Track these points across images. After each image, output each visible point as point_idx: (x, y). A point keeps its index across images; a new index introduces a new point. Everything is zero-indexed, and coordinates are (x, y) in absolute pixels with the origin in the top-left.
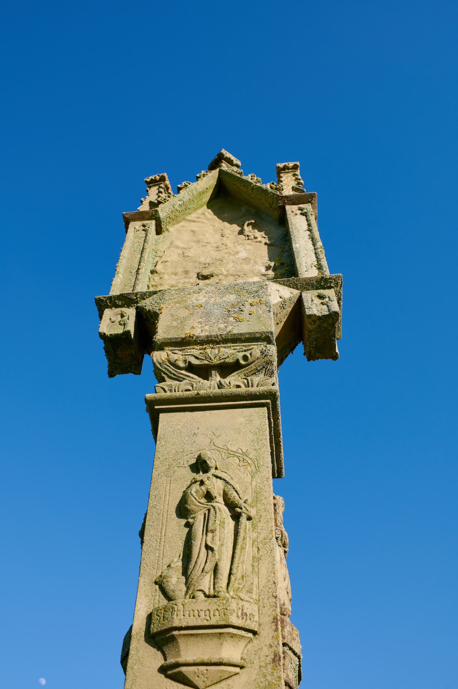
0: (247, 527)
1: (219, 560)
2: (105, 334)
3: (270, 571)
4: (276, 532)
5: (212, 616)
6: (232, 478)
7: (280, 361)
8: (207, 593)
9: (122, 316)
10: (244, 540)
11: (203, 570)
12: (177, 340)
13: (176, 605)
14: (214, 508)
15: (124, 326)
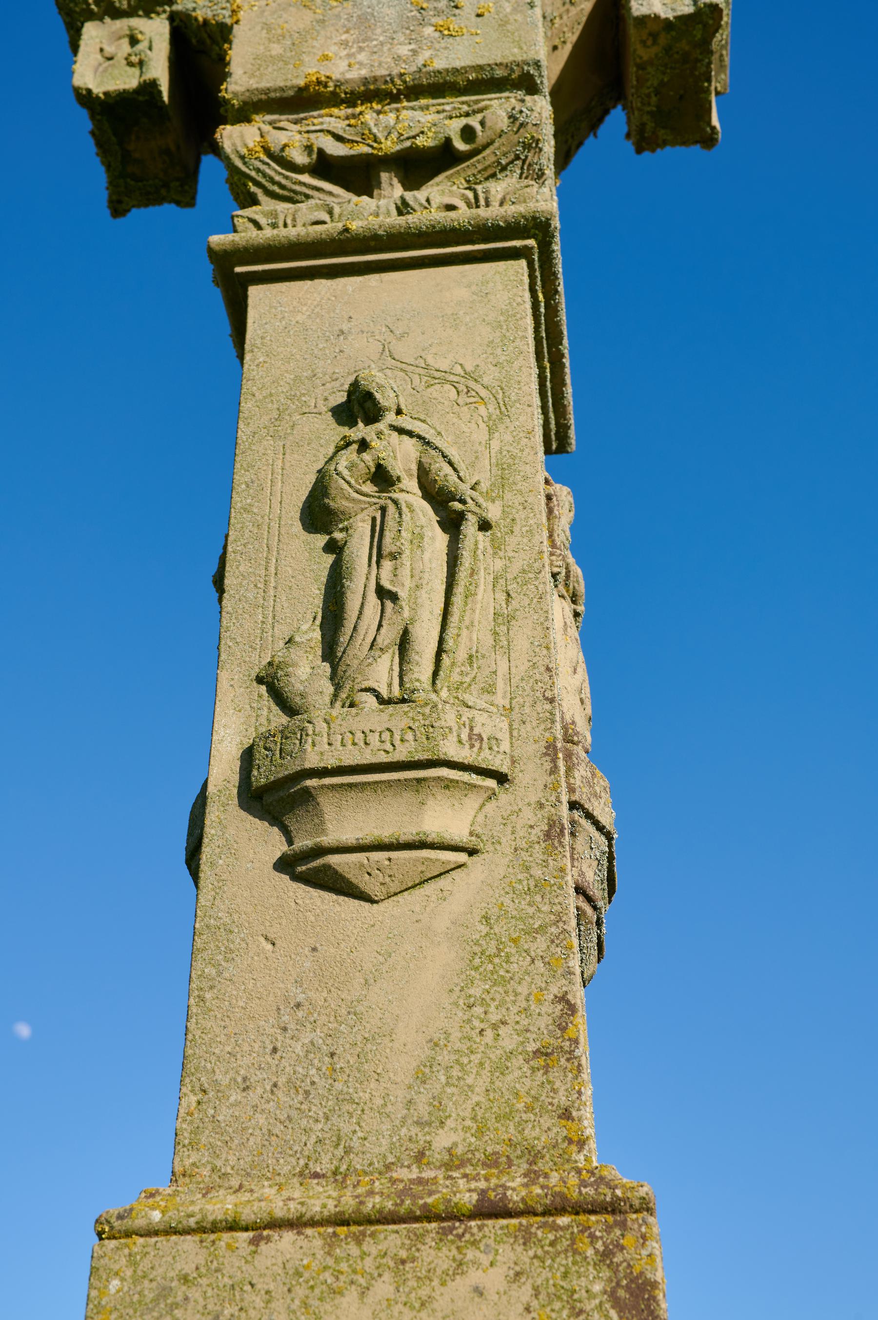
0: (481, 546)
1: (412, 620)
2: (89, 91)
3: (536, 644)
4: (552, 561)
5: (397, 743)
6: (439, 433)
7: (563, 159)
8: (385, 694)
9: (134, 41)
10: (472, 575)
11: (372, 645)
12: (285, 95)
13: (309, 722)
14: (395, 502)
15: (141, 68)
